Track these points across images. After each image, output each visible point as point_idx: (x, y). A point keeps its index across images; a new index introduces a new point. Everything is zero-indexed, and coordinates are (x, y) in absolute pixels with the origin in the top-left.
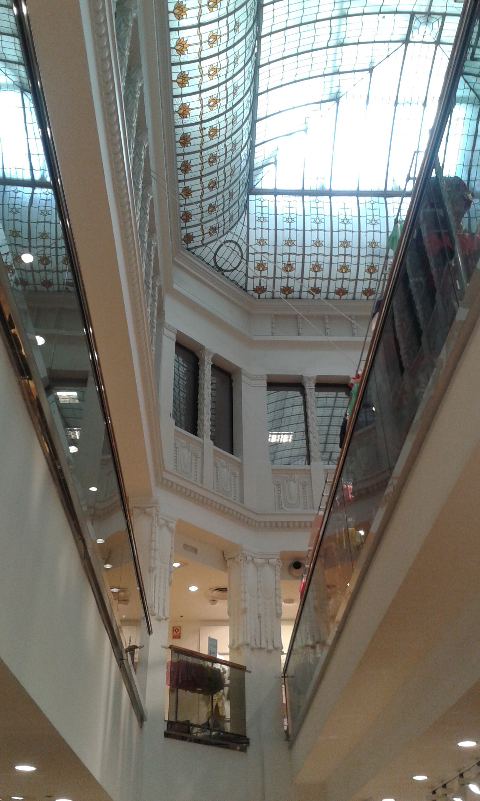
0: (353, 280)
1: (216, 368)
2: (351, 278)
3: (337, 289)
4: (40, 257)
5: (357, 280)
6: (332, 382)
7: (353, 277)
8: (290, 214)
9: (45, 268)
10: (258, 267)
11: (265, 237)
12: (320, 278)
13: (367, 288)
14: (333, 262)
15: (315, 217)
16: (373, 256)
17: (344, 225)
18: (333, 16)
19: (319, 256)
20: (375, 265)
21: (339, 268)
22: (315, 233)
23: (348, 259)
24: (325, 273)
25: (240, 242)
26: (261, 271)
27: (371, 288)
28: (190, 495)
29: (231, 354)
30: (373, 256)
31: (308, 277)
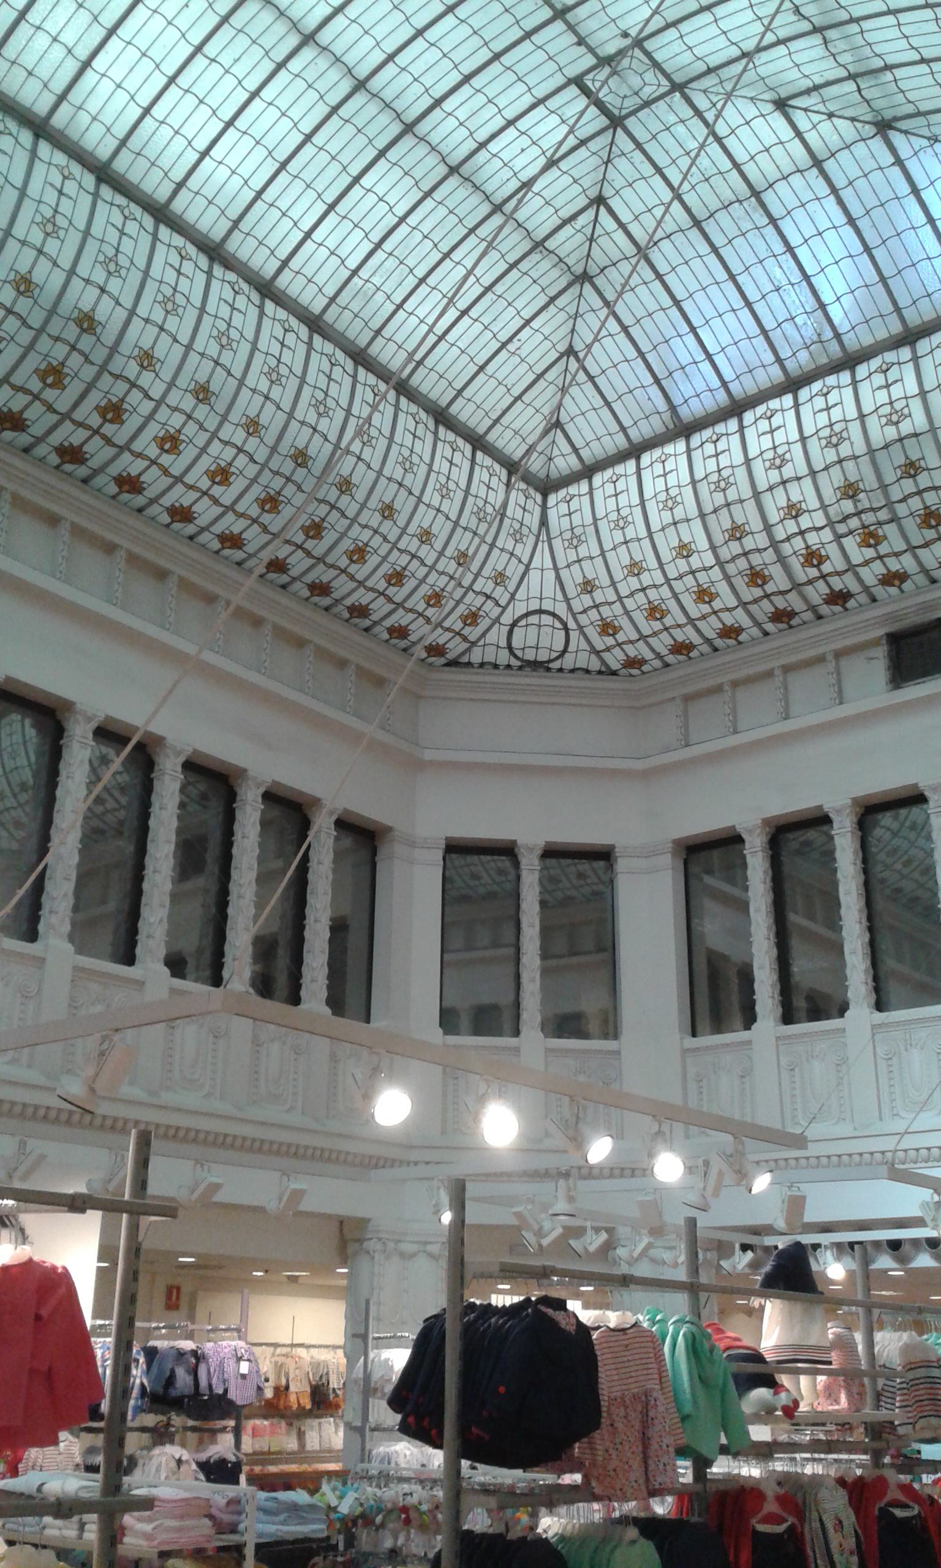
0: (313, 557)
1: (271, 797)
2: (115, 440)
3: (66, 444)
4: (50, 363)
5: (179, 479)
6: (31, 696)
7: (176, 471)
8: (56, 211)
9: (40, 392)
10: (163, 439)
11: (159, 353)
12: (44, 402)
13: (185, 505)
14: (99, 384)
15: (168, 292)
16: (288, 479)
17: (42, 235)
18: (691, 113)
19: (241, 455)
20: (125, 406)
21: (103, 404)
22: (307, 432)
23: (377, 541)
24: (63, 401)
25: (547, 605)
26: (105, 420)
27: (25, 416)
28: (260, 1148)
29: (337, 784)
30: (288, 479)
31: (191, 483)
